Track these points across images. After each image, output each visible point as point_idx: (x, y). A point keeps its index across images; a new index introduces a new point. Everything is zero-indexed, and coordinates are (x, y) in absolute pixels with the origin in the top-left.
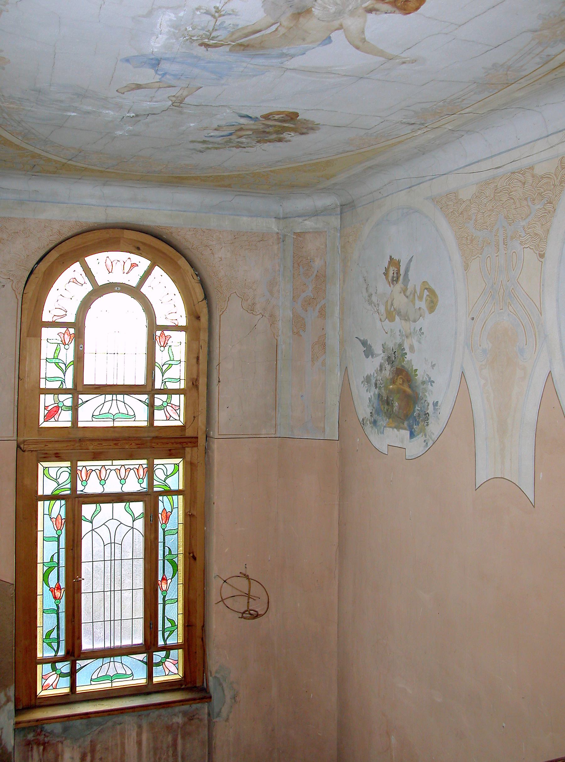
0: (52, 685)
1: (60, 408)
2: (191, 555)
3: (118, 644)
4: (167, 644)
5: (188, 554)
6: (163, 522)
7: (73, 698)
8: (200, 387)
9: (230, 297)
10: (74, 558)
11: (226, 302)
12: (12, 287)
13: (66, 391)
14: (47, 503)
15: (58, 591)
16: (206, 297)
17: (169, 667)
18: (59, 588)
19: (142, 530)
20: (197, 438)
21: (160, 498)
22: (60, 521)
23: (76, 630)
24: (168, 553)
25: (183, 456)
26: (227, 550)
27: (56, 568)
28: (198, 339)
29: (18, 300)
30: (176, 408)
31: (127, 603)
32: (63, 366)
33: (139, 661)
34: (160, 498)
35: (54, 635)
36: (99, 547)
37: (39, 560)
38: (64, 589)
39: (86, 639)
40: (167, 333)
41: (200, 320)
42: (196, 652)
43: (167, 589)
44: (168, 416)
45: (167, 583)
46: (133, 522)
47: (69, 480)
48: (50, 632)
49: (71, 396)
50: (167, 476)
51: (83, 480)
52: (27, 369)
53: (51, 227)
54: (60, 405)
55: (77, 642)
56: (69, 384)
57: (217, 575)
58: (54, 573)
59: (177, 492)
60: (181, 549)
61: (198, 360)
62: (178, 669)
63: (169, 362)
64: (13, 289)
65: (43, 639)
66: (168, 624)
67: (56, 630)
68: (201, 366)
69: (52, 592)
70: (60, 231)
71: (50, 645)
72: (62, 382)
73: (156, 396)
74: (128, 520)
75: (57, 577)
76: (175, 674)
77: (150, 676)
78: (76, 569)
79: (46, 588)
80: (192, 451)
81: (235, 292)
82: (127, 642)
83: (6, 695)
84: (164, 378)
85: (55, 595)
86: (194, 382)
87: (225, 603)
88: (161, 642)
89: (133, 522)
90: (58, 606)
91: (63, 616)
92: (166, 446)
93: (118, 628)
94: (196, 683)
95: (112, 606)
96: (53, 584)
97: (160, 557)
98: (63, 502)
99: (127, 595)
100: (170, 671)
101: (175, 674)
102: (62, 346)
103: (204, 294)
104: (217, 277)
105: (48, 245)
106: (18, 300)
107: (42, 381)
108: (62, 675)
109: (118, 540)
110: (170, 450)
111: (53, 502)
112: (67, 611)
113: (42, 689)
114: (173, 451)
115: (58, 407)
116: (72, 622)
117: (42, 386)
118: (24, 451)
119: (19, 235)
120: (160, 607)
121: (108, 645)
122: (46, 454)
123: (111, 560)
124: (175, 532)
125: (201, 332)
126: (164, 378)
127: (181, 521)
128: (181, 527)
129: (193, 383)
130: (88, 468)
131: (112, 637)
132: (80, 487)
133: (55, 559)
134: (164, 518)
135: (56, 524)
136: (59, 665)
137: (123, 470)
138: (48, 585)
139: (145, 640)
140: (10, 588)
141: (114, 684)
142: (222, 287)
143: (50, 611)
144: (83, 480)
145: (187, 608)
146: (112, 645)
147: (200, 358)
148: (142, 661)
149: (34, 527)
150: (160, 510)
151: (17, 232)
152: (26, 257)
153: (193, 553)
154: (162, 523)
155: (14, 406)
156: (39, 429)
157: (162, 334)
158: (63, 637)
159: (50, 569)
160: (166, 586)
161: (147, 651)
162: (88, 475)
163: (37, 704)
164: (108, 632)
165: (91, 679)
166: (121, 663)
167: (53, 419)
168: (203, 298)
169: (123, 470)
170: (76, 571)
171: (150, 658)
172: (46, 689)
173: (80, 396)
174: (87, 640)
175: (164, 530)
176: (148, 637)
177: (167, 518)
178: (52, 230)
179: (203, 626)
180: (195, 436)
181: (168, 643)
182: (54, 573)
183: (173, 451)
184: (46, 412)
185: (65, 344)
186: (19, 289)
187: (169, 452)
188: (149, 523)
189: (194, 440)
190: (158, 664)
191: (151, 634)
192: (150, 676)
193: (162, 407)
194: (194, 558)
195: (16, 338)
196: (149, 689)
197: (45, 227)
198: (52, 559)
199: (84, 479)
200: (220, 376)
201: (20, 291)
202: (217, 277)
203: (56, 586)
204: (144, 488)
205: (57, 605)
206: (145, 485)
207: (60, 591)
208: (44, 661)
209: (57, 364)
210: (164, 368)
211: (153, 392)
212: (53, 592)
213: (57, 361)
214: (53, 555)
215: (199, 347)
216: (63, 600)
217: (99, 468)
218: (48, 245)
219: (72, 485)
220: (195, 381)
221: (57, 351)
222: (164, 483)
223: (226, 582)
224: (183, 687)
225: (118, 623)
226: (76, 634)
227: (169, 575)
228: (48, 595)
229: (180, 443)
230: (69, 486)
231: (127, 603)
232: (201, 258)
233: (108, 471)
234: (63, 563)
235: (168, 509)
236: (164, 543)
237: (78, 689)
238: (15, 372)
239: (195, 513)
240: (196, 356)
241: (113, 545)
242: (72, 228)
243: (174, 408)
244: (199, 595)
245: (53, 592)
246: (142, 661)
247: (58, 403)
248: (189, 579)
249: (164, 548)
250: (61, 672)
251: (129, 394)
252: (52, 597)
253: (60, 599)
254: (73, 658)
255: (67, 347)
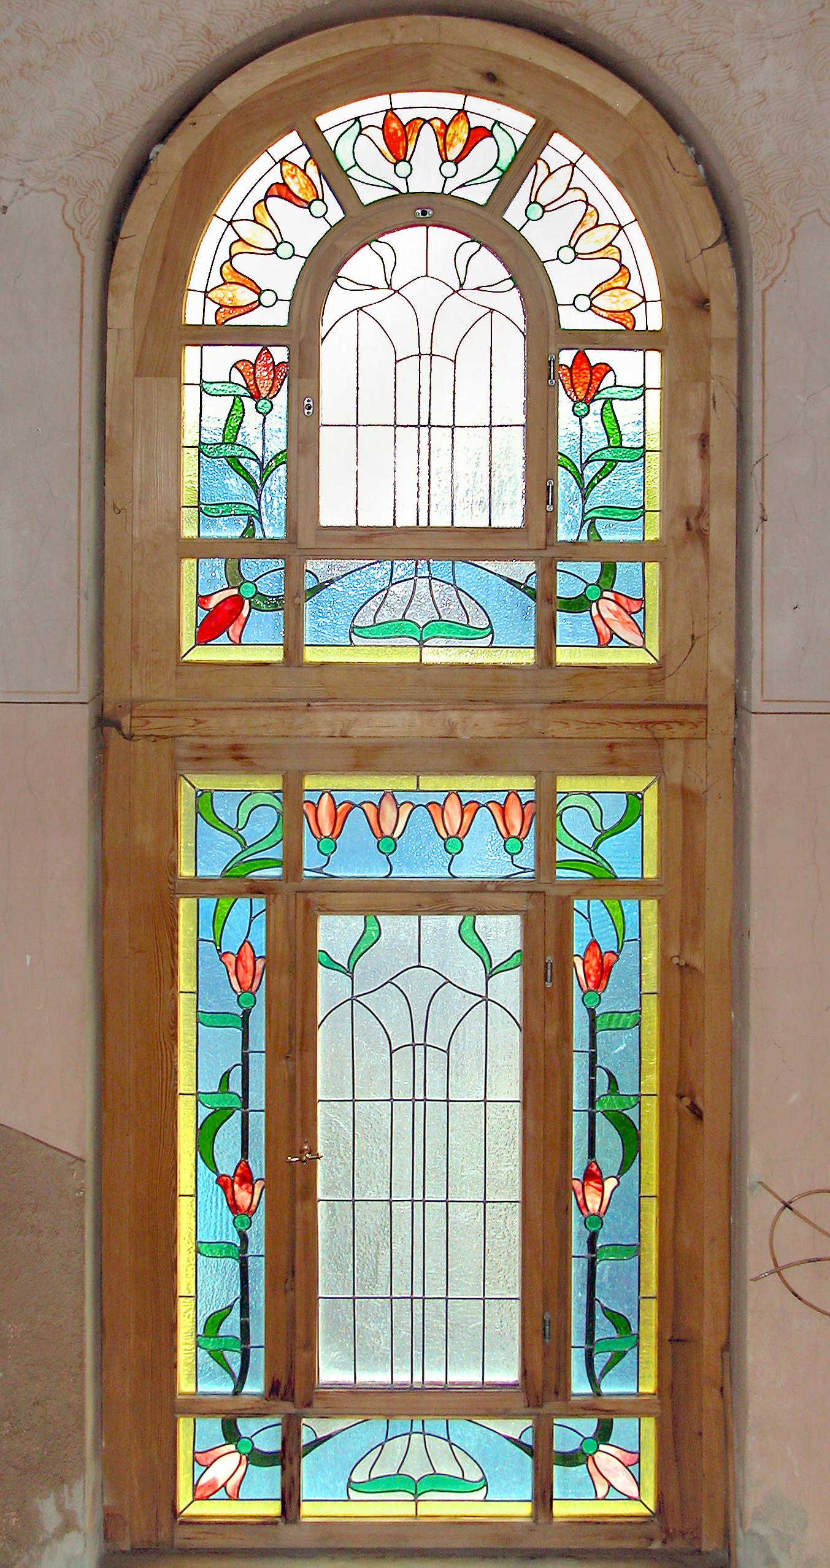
0: (224, 1485)
1: (247, 602)
2: (687, 1101)
3: (435, 1375)
4: (599, 1394)
5: (674, 1099)
6: (590, 984)
7: (288, 1535)
8: (714, 536)
9: (798, 225)
10: (292, 1085)
11: (785, 244)
12: (63, 216)
13: (266, 549)
14: (207, 904)
15: (243, 1187)
16: (729, 233)
17: (609, 1470)
18: (245, 1176)
19: (517, 1010)
20: (706, 707)
21: (579, 904)
22: (250, 963)
23: (300, 1321)
24: (606, 1089)
25: (658, 771)
26: (794, 1097)
27: (238, 1113)
28: (703, 376)
29: (83, 257)
30: (631, 607)
31: (467, 1248)
32: (253, 467)
33: (507, 1443)
34: (579, 904)
35: (232, 1325)
36: (372, 1057)
37: (185, 1083)
38: (263, 1183)
39: (331, 1349)
40: (595, 357)
41: (708, 311)
42: (701, 1434)
43: (603, 1210)
44: (605, 631)
45: (602, 1191)
46: (488, 979)
47: (278, 835)
48: (216, 1320)
49: (281, 564)
50: (604, 834)
51: (451, 834)
52: (137, 479)
53: (180, 18)
54: (248, 591)
55: (301, 1356)
56: (273, 529)
57: (761, 1183)
58: (231, 1129)
59: (639, 888)
60: (652, 1081)
61: (704, 446)
62: (638, 1484)
63: (606, 455)
64: (67, 224)
65: (197, 1336)
66: (604, 1328)
67: (236, 1312)
68: (714, 469)
69: (225, 1189)
70: (209, 32)
71: (218, 1357)
72: (250, 521)
73: (560, 565)
74: (471, 973)
75: (239, 1144)
76: (630, 1498)
77: (543, 1496)
78: (298, 1123)
79: (207, 1176)
80: (686, 750)
81: (818, 210)
82: (466, 1374)
83: (60, 1508)
84: (588, 508)
85: (233, 1198)
86: (692, 521)
87: (788, 1280)
88: (580, 1386)
89: (488, 979)
90: (244, 1238)
91: (258, 1267)
92: (600, 732)
93: (435, 1322)
94: (698, 1538)
95: (418, 1251)
96: (227, 1165)
97: (579, 1098)
98: (260, 903)
99: (465, 1216)
100: (610, 1485)
101: (630, 1498)
102: (249, 403)
103: (719, 224)
104: (749, 158)
105: (173, 76)
106: (83, 257)
107: (188, 516)
108: (257, 1458)
109: (438, 1035)
110: (611, 746)
111: (225, 903)
112: (270, 1257)
113: (194, 1494)
114: (622, 752)
115: (236, 602)
116: (286, 1291)
117: (189, 531)
118: (130, 737)
119: (79, 50)
120: (577, 1270)
121: (402, 1377)
122: (204, 747)
123: (425, 1100)
124: (631, 1019)
125: (714, 350)
126: (588, 508)
127: (651, 983)
128: (651, 1008)
129: (688, 524)
130: (339, 797)
131: (417, 1353)
132: (311, 858)
133: (236, 1086)
134: (591, 972)
135: (236, 974)
136: (246, 1426)
137: (453, 809)
138: (212, 1165)
139: (524, 1373)
140: (73, 1171)
141: (425, 1509)
142: (768, 193)
143: (221, 1248)
144: (512, 834)
145: (669, 1279)
146: (417, 1378)
147: (713, 439)
148: (518, 1443)
149: (167, 978)
150: (579, 946)
151: (74, 41)
152: (103, 118)
153: (692, 1095)
154: (585, 988)
155: (79, 593)
156: (179, 668)
157: (581, 357)
158: (258, 1334)
159: (219, 1116)
160: (599, 1200)
161: (530, 1410)
162: (338, 820)
163: (178, 1542)
164: (402, 1333)
165: (350, 1481)
166: (448, 1440)
167: (223, 638)
168: (719, 235)
169: (453, 809)
170: (299, 1130)
171: (544, 1431)
172: (207, 1498)
173: (310, 565)
174: (334, 1355)
175: (591, 1012)
176: (537, 1365)
177: (604, 972)
178: (184, 27)
179: (726, 1347)
180: (700, 701)
181: (604, 1389)
182: (231, 1129)
183: (622, 752)
184: (203, 614)
185: (256, 397)
186: (85, 222)
187: (605, 752)
188: (540, 986)
189: (694, 715)
190: (570, 1459)
191: (545, 1355)
192: (543, 1496)
193: (578, 604)
194: (697, 1113)
195: (80, 379)
196: (538, 1542)
197: (160, 19)
198: (224, 1083)
199: (327, 833)
200: (766, 498)
201: (89, 227)
202: (749, 158)
203: (239, 1171)
204: (525, 870)
205: (239, 1232)
206: (527, 858)
207: (251, 1188)
208: (198, 1407)
209: (234, 463)
210: (589, 473)
211: (549, 553)
212: (229, 1191)
213: (237, 451)
214: (229, 1072)
215: (708, 402)
216: (260, 1218)
217: (375, 798)
218: (173, 76)
219: (286, 851)
220: (695, 514)
221: (234, 422)
222: (593, 854)
223: (791, 1209)
224: (656, 1545)
225: (438, 1308)
226: (300, 1332)
227: (609, 1161)
228: (213, 1197)
229: (646, 724)
230: (277, 853)
231: (467, 1248)
232: (693, 96)
233: (405, 811)
234: (258, 1097)
235: (607, 944)
236: (593, 1057)
237: (307, 1510)
238: (80, 487)
239: (697, 961)
240: (697, 431)
241: (419, 1050)
242: (248, 15)
243: (626, 607)
244: (713, 1240)
245: (229, 1191)
246: (518, 1443)
247: (239, 588)
248: (679, 1182)
249: (592, 1071)
250: (253, 1449)
251: (469, 558)
252: (225, 1204)
253: (250, 1212)
254: (288, 1407)
255: (264, 405)
